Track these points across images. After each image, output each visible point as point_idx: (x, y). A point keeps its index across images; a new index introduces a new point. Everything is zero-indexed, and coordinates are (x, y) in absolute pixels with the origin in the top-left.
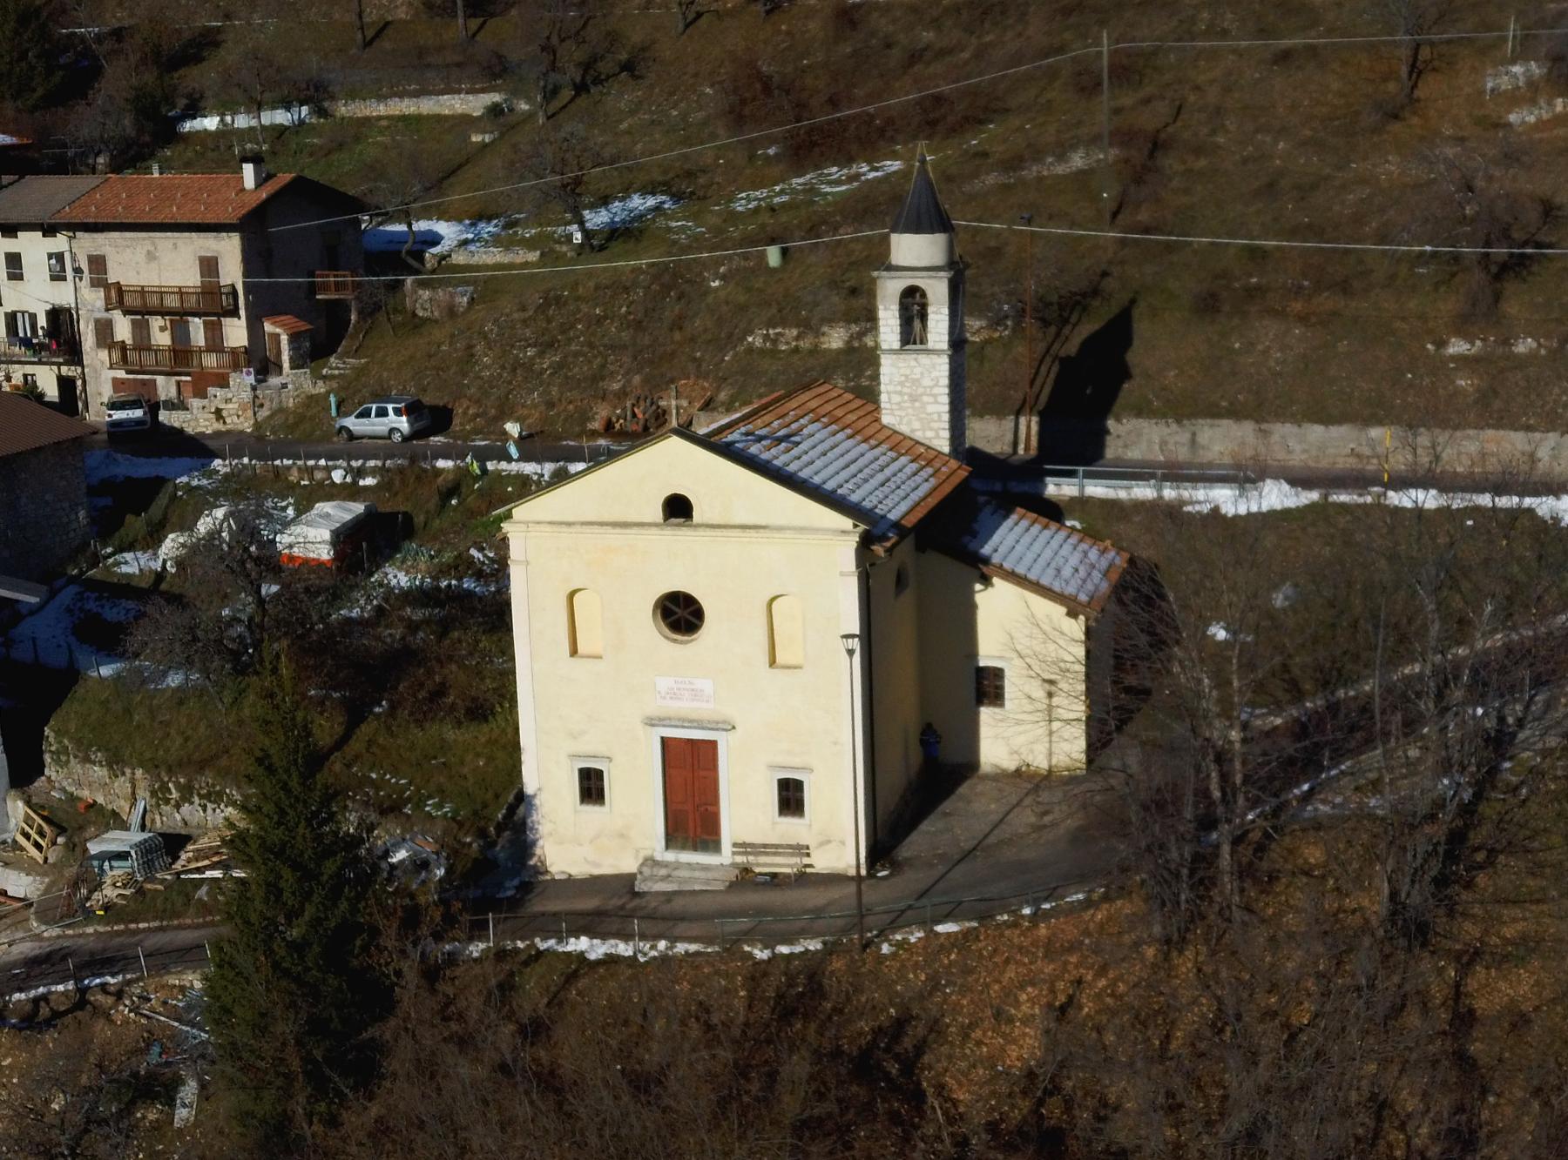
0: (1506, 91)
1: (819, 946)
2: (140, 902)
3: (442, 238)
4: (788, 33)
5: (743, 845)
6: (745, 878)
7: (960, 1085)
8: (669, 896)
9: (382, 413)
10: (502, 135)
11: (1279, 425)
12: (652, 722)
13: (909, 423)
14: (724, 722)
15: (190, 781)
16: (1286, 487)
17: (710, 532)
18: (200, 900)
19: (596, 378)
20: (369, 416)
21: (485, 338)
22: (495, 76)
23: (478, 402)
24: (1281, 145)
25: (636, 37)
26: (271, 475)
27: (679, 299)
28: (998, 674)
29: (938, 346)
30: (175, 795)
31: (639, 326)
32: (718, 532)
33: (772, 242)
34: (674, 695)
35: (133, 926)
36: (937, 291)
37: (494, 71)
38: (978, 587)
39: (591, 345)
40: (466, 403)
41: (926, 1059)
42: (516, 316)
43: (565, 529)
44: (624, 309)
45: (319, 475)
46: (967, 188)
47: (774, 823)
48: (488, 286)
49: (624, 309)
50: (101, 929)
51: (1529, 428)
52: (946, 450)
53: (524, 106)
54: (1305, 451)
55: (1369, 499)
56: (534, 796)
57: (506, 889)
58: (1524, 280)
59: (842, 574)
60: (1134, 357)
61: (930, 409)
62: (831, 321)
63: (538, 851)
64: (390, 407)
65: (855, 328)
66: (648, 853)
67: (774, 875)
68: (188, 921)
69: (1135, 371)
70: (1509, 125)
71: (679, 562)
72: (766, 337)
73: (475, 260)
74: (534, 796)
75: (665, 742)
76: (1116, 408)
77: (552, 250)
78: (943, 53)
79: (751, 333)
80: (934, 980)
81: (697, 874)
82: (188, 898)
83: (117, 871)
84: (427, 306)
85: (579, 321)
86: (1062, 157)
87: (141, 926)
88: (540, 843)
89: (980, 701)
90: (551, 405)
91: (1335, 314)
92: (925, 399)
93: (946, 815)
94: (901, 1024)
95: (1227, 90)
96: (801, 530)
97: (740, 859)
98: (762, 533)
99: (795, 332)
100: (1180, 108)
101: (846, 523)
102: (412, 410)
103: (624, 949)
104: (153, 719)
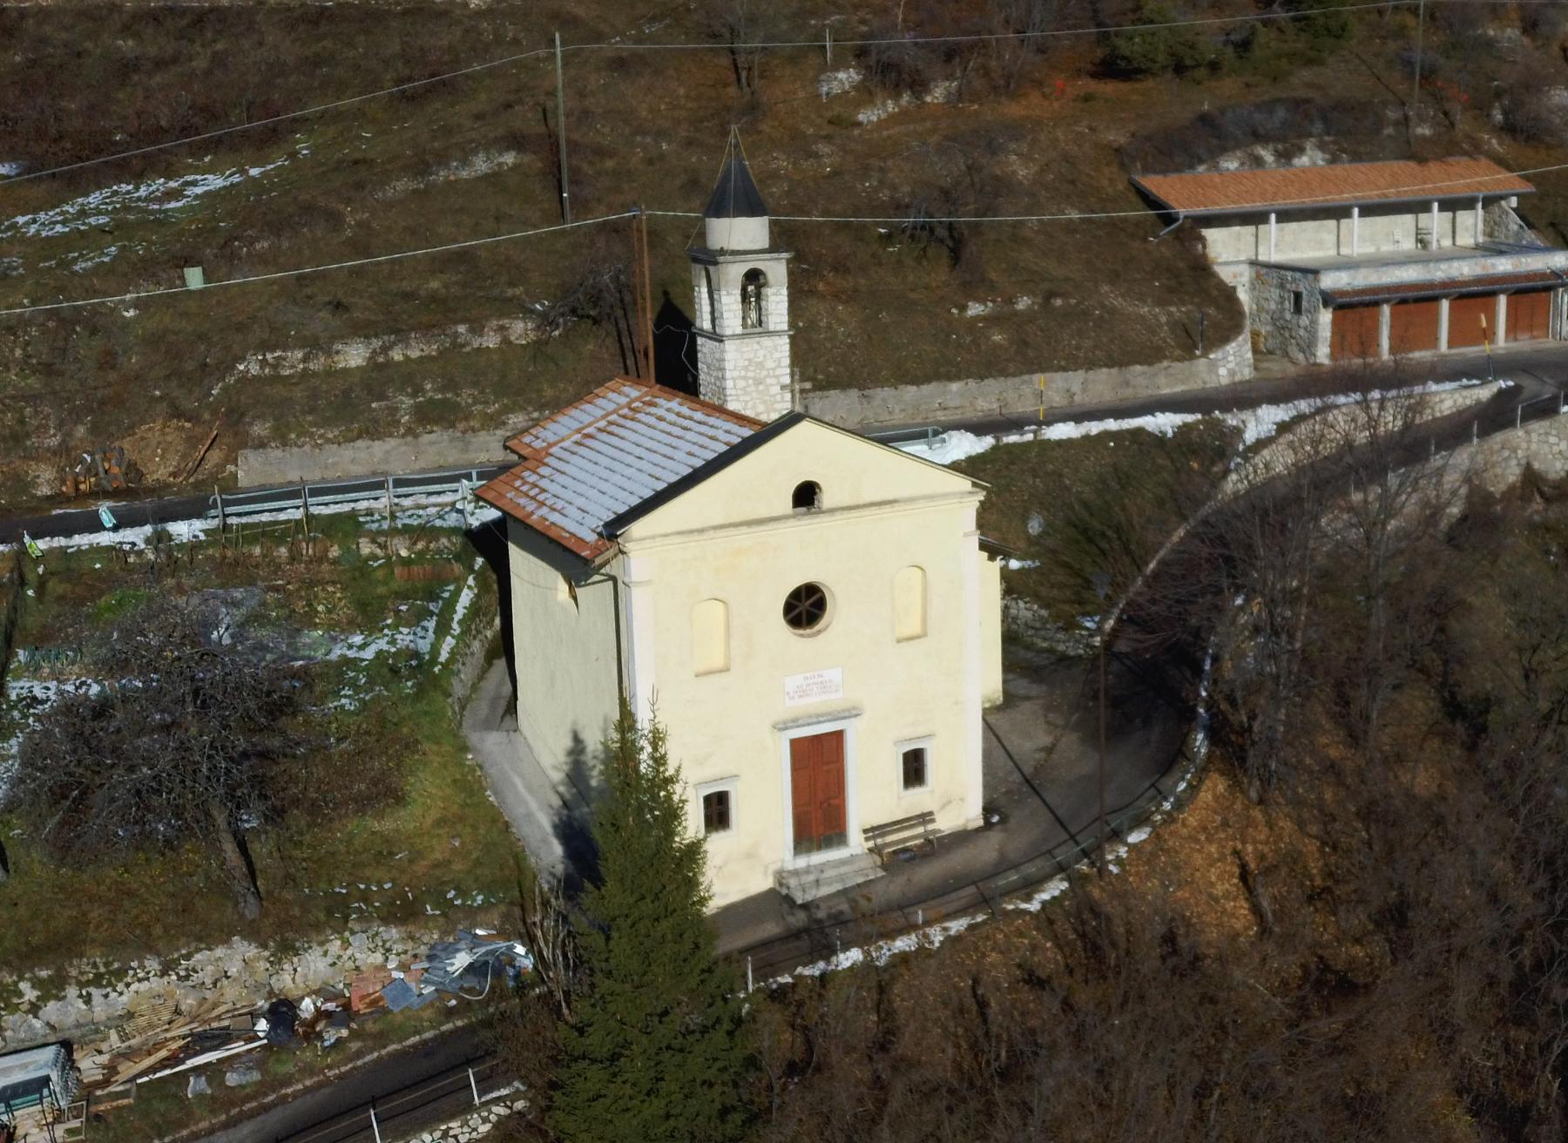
5: (873, 829)
6: (897, 860)
13: (754, 407)
16: (970, 436)
17: (846, 515)
18: (200, 1096)
29: (778, 328)
30: (30, 994)
31: (48, 370)
32: (854, 513)
33: (189, 262)
34: (803, 693)
36: (777, 270)
43: (696, 537)
44: (18, 352)
49: (18, 352)
54: (902, 410)
55: (1029, 437)
65: (376, 343)
68: (204, 1125)
70: (859, 124)
71: (804, 554)
72: (264, 363)
75: (795, 743)
79: (242, 359)
81: (843, 870)
82: (182, 1100)
86: (465, 162)
92: (769, 381)
96: (930, 497)
97: (871, 844)
98: (897, 507)
99: (299, 354)
100: (544, 111)
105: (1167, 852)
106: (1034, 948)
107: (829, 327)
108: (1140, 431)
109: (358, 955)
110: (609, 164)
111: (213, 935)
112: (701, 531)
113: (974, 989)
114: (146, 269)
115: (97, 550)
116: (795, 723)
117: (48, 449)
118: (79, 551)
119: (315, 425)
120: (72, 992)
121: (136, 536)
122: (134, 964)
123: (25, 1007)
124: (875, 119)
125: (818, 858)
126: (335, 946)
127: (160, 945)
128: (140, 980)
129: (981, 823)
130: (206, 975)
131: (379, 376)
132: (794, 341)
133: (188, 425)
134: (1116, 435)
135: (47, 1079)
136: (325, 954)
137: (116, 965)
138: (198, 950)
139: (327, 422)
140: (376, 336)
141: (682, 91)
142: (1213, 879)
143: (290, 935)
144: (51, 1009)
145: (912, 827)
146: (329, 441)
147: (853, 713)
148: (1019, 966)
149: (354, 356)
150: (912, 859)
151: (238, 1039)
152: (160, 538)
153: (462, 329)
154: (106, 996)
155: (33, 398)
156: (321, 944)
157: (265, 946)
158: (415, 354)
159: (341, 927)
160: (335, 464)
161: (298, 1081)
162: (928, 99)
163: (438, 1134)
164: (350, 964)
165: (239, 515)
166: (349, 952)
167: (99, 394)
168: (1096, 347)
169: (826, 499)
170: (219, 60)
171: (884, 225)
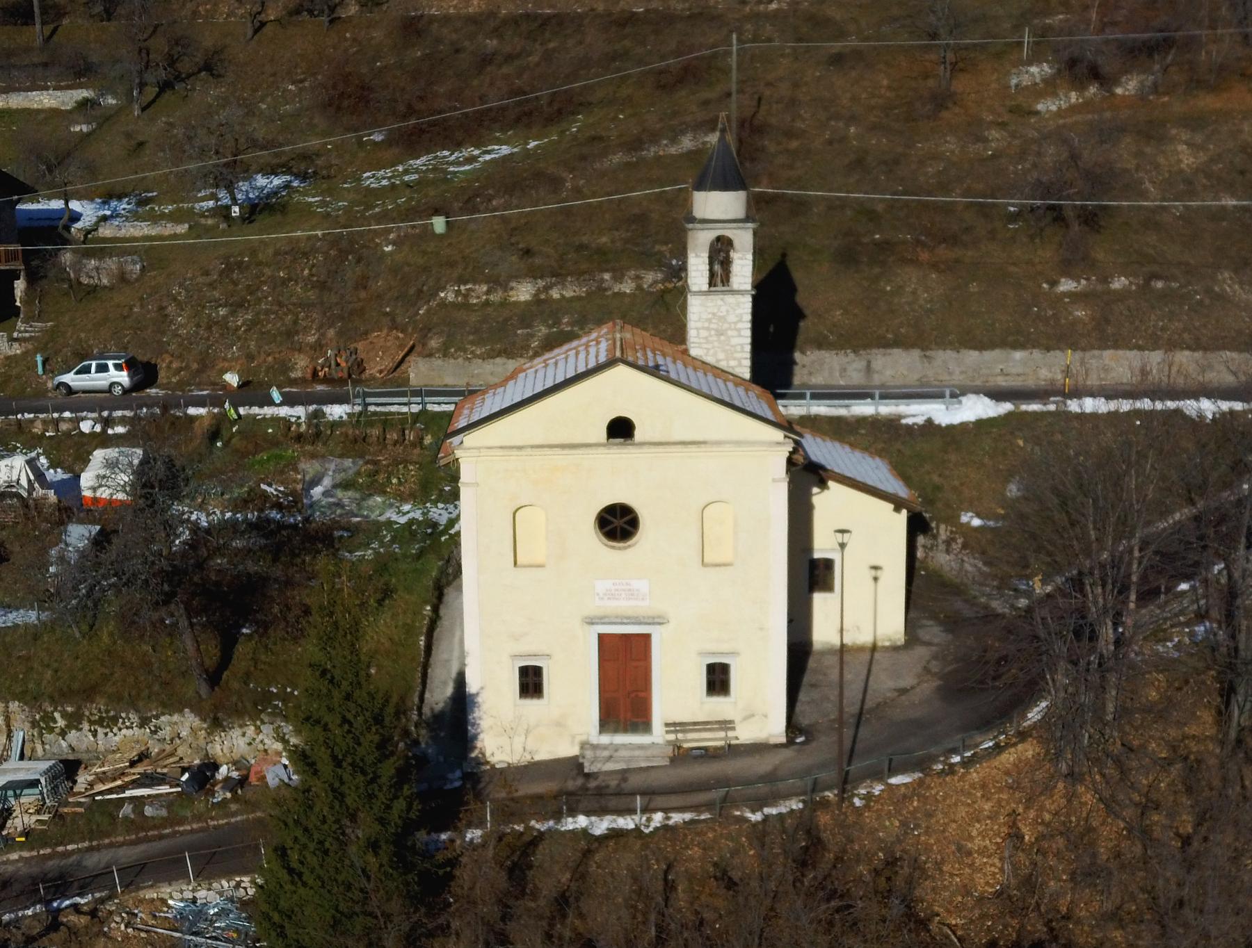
0: (1027, 87)
1: (801, 805)
2: (61, 825)
3: (81, 215)
4: (354, 40)
5: (674, 724)
6: (680, 756)
7: (948, 911)
8: (624, 774)
9: (103, 368)
10: (100, 126)
11: (941, 353)
12: (591, 622)
13: (715, 354)
14: (659, 617)
15: (79, 708)
16: (987, 400)
19: (290, 334)
20: (90, 372)
21: (175, 299)
22: (79, 74)
23: (180, 357)
24: (852, 130)
25: (208, 41)
26: (14, 428)
27: (359, 261)
28: (828, 564)
30: (61, 723)
31: (322, 286)
32: (661, 449)
33: (437, 212)
35: (60, 849)
36: (743, 240)
37: (80, 72)
38: (815, 490)
39: (280, 304)
40: (168, 359)
41: (918, 892)
42: (200, 279)
43: (515, 452)
44: (306, 272)
45: (64, 427)
46: (597, 165)
47: (702, 703)
48: (154, 256)
49: (306, 272)
50: (26, 854)
51: (1140, 348)
52: (747, 376)
53: (111, 101)
54: (962, 372)
55: (1052, 407)
56: (477, 694)
57: (452, 781)
58: (1098, 232)
59: (774, 480)
60: (801, 299)
61: (734, 341)
62: (518, 277)
63: (479, 744)
64: (110, 363)
65: (541, 283)
66: (584, 738)
67: (706, 749)
68: (120, 839)
69: (807, 312)
70: (1037, 113)
72: (458, 293)
73: (122, 233)
74: (477, 694)
75: (602, 637)
76: (800, 339)
77: (197, 224)
78: (509, 58)
79: (443, 289)
80: (904, 824)
81: (637, 753)
82: (113, 818)
83: (29, 798)
84: (94, 274)
85: (265, 283)
87: (70, 847)
88: (481, 737)
89: (812, 589)
90: (250, 357)
91: (957, 261)
92: (730, 333)
93: (814, 686)
94: (891, 862)
95: (796, 85)
96: (738, 443)
97: (672, 737)
100: (760, 99)
101: (779, 435)
102: (131, 365)
103: (626, 823)
104: (9, 655)
105: (924, 799)
106: (735, 852)
107: (914, 293)
108: (1178, 412)
109: (266, 741)
110: (794, 144)
111: (174, 705)
112: (520, 448)
113: (666, 873)
114: (409, 214)
115: (276, 420)
116: (601, 620)
117: (308, 344)
118: (264, 419)
119: (472, 343)
120: (86, 726)
121: (300, 411)
122: (123, 715)
123: (57, 730)
124: (1054, 108)
125: (621, 739)
126: (251, 730)
127: (141, 704)
128: (127, 728)
129: (783, 740)
130: (166, 733)
131: (540, 307)
132: (756, 301)
133: (401, 335)
134: (1148, 415)
135: (38, 781)
136: (244, 735)
137: (112, 713)
138: (163, 714)
139: (479, 342)
140: (541, 278)
141: (885, 82)
142: (974, 833)
143: (220, 715)
144: (73, 735)
145: (710, 730)
146: (476, 356)
147: (659, 621)
148: (715, 865)
149: (523, 292)
150: (701, 756)
151: (166, 784)
152: (318, 415)
153: (607, 276)
154: (106, 734)
155: (306, 305)
156: (241, 726)
157: (204, 720)
158: (569, 294)
159: (255, 716)
160: (478, 375)
161: (189, 823)
162: (1119, 91)
163: (233, 883)
164: (261, 747)
165: (377, 405)
166: (261, 737)
167: (350, 306)
168: (1185, 330)
169: (639, 435)
170: (548, 57)
171: (1013, 205)
